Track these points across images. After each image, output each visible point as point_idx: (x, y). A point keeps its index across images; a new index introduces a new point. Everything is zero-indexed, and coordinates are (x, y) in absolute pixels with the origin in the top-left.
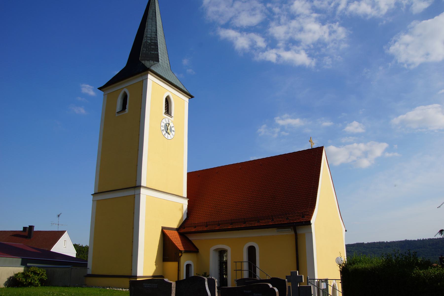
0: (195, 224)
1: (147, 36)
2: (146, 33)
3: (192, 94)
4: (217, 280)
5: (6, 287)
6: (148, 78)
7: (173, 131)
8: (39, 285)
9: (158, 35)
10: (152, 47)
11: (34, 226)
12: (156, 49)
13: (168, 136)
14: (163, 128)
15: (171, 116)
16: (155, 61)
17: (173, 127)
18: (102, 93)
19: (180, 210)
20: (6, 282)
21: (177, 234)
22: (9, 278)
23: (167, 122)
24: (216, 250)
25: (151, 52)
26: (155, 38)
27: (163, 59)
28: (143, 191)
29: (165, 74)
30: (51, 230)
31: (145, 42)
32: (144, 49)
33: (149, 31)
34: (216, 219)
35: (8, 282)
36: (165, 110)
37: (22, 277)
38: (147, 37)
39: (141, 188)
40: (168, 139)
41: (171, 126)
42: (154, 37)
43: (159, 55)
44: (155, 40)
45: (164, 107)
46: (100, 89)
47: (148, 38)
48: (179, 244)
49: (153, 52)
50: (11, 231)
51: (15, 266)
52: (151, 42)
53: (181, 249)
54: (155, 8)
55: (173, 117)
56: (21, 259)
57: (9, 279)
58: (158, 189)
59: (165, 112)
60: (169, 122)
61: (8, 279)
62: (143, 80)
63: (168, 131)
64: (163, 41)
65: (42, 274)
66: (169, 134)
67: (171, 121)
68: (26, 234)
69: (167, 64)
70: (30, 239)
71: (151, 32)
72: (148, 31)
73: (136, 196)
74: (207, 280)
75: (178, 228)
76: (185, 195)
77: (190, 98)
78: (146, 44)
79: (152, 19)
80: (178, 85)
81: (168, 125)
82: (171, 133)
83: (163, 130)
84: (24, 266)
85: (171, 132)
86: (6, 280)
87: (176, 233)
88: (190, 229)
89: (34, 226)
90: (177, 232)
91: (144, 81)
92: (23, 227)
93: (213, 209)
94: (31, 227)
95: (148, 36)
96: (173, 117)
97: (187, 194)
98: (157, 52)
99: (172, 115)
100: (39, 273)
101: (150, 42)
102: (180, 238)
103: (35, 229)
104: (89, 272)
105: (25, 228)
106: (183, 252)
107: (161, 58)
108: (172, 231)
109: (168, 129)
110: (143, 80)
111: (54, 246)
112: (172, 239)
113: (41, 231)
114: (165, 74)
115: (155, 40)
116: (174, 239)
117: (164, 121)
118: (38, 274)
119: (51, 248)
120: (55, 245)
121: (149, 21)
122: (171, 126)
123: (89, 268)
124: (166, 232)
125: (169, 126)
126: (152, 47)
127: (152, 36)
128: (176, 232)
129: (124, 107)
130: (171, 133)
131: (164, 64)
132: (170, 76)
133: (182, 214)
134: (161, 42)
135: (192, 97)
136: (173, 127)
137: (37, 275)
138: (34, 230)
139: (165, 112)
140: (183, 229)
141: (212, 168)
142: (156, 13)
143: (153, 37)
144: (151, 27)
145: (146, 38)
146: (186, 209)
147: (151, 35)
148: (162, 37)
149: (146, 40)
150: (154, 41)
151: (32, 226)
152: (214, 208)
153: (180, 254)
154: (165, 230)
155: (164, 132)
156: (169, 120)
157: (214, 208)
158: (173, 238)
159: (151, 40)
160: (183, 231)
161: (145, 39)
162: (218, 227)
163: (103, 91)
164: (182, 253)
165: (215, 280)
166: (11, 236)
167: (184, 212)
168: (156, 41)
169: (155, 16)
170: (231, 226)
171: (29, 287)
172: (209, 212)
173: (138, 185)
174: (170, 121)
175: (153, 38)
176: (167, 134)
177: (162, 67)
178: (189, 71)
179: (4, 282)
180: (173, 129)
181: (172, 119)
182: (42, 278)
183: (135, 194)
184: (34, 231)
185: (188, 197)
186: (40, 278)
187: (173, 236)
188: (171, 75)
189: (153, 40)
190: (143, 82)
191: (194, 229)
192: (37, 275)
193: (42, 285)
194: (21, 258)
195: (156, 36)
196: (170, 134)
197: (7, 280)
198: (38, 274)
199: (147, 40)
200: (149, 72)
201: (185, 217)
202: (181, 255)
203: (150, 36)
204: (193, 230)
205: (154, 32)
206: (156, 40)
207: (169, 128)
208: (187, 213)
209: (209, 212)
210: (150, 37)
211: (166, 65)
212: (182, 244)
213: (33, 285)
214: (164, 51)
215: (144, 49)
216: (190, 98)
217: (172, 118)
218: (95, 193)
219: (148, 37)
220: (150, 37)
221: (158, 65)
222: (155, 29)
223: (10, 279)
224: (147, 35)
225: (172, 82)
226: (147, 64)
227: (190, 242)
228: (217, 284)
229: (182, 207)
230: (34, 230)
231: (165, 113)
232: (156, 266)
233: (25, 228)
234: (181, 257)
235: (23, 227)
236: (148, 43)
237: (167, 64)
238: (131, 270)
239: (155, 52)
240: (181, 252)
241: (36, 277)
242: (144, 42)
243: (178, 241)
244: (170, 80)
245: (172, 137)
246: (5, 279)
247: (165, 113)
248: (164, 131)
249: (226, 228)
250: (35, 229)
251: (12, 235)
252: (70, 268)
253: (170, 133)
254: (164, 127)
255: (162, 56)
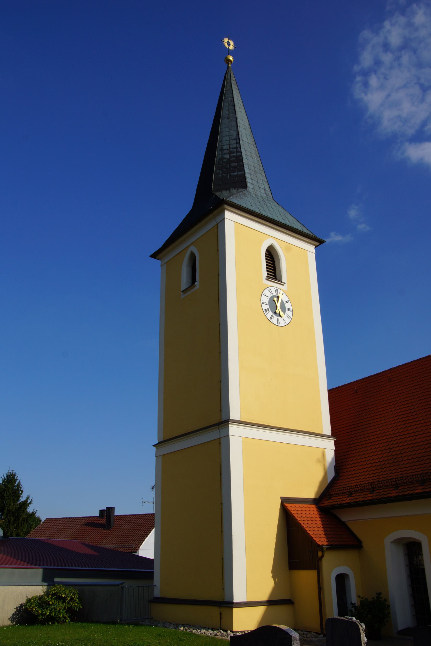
0: (350, 489)
1: (223, 148)
2: (221, 144)
3: (319, 237)
4: (364, 627)
5: (15, 623)
6: (224, 218)
7: (289, 310)
8: (67, 621)
9: (241, 142)
10: (233, 164)
11: (114, 508)
12: (241, 167)
13: (278, 321)
14: (266, 307)
15: (281, 281)
16: (239, 188)
17: (287, 302)
18: (157, 263)
19: (319, 461)
20: (13, 614)
21: (315, 510)
22: (19, 607)
23: (274, 294)
24: (398, 542)
25: (231, 174)
26: (236, 148)
27: (255, 183)
28: (233, 429)
29: (260, 208)
30: (68, 517)
31: (220, 159)
32: (218, 171)
33: (226, 138)
34: (396, 473)
35: (18, 615)
36: (266, 273)
37: (36, 606)
38: (222, 150)
39: (229, 424)
40: (279, 325)
41: (282, 301)
42: (235, 148)
43: (247, 175)
44: (237, 152)
45: (265, 266)
46: (154, 256)
47: (224, 152)
48: (317, 532)
49: (236, 174)
50: (83, 517)
51: (29, 584)
52: (230, 156)
53: (319, 543)
54: (232, 99)
55: (285, 283)
56: (41, 571)
57: (19, 608)
58: (267, 424)
59: (268, 277)
60: (277, 294)
61: (17, 610)
62: (217, 224)
63: (277, 311)
64: (253, 152)
65: (72, 599)
66: (280, 316)
67: (282, 292)
68: (103, 521)
69: (265, 190)
70: (110, 530)
71: (229, 140)
72: (223, 140)
73: (223, 440)
74: (298, 638)
75: (317, 497)
76: (328, 431)
77: (317, 244)
78: (221, 163)
79: (229, 118)
80: (288, 223)
81: (275, 299)
82: (284, 314)
83: (267, 310)
84: (46, 584)
85: (284, 311)
86: (14, 611)
87: (312, 509)
88: (341, 500)
89: (114, 508)
90: (314, 506)
91: (219, 224)
92: (99, 510)
93: (385, 455)
94: (110, 510)
95: (224, 147)
96: (285, 283)
97: (332, 430)
98: (243, 172)
99: (284, 280)
100: (65, 597)
101: (228, 158)
102: (320, 518)
103: (117, 513)
104: (157, 593)
105: (101, 511)
106: (325, 549)
107: (251, 181)
108: (300, 505)
109: (277, 307)
110: (217, 224)
111: (146, 540)
112: (301, 522)
113: (126, 515)
114: (260, 208)
115: (237, 152)
116: (306, 522)
117: (266, 292)
118: (64, 600)
119: (141, 543)
120: (147, 538)
121: (224, 122)
122: (282, 301)
123: (155, 586)
124: (290, 509)
125: (278, 302)
126: (233, 164)
127: (231, 146)
128: (313, 507)
129: (193, 280)
130: (284, 314)
131: (259, 190)
132: (272, 210)
133: (325, 469)
134: (249, 154)
135: (321, 242)
136: (287, 302)
137: (62, 601)
138: (115, 514)
139: (267, 275)
140: (327, 500)
141: (380, 372)
142: (236, 107)
143: (232, 148)
144: (229, 131)
145: (220, 153)
146: (332, 459)
147: (229, 145)
148: (250, 145)
149: (221, 156)
150: (235, 154)
151: (111, 508)
152: (388, 451)
153: (320, 554)
154: (286, 505)
155: (270, 314)
156: (277, 290)
157: (388, 451)
158: (305, 519)
159: (230, 153)
160: (328, 504)
161: (220, 155)
162: (396, 491)
163: (160, 260)
164: (323, 552)
165: (360, 627)
166: (82, 525)
167: (327, 465)
168: (240, 153)
169: (234, 111)
170: (421, 488)
171: (49, 624)
172: (377, 461)
173: (224, 418)
174: (279, 290)
175: (234, 149)
176: (275, 317)
177: (254, 196)
178: (361, 227)
179: (10, 615)
180: (288, 306)
181: (284, 287)
182: (70, 606)
183: (220, 437)
184: (116, 516)
185: (334, 434)
186: (68, 607)
187: (304, 516)
188: (273, 209)
189: (234, 153)
190: (217, 227)
191: (349, 498)
192: (62, 601)
193: (72, 620)
194: (42, 568)
195: (238, 145)
196: (282, 315)
197: (16, 610)
198: (64, 600)
199: (223, 155)
200: (226, 206)
201: (332, 475)
202: (323, 556)
203: (227, 147)
204: (347, 500)
205: (234, 139)
206: (239, 152)
207: (278, 305)
208: (335, 467)
209: (377, 461)
210: (227, 150)
211: (263, 191)
212: (323, 532)
213: (58, 621)
214: (256, 169)
215: (218, 171)
216: (318, 244)
217: (283, 285)
218: (159, 441)
219: (224, 150)
220: (228, 148)
221: (244, 194)
222: (235, 133)
223: (20, 609)
224: (222, 147)
225: (276, 218)
226: (223, 195)
227: (344, 525)
228: (366, 636)
229: (324, 455)
230: (115, 514)
231: (268, 278)
232: (275, 580)
233: (101, 511)
234: (323, 559)
235: (99, 510)
236: (225, 160)
237: (265, 190)
238: (223, 589)
239: (239, 173)
240: (320, 548)
241: (60, 605)
242: (218, 159)
243: (315, 526)
244: (270, 216)
245: (288, 321)
246: (11, 610)
247: (268, 278)
248: (270, 311)
249: (410, 493)
250: (117, 513)
251: (84, 525)
252: (120, 587)
253: (282, 314)
254: (268, 303)
255: (252, 177)
